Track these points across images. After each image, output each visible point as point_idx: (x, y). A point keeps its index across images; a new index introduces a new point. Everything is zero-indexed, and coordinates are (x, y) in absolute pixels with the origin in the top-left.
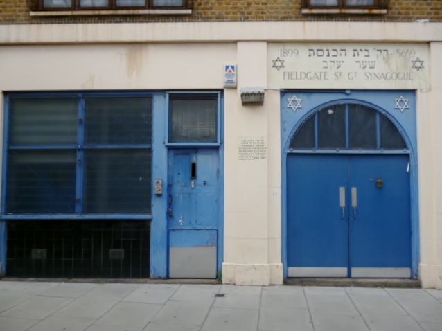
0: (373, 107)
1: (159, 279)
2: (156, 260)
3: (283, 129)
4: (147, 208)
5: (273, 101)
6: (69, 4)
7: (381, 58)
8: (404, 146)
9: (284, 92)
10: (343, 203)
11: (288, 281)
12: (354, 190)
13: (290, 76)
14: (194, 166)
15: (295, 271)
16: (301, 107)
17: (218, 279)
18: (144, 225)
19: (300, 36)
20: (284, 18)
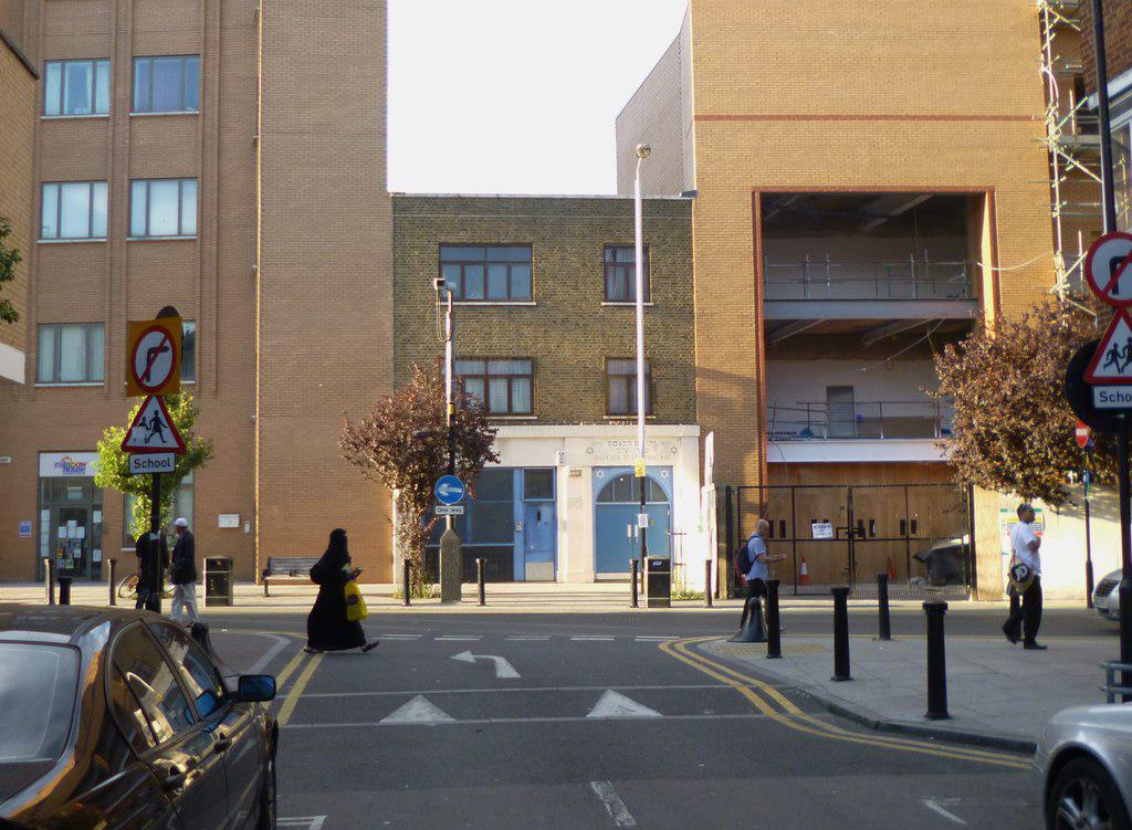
0: (759, 229)
1: (520, 581)
2: (517, 571)
3: (594, 490)
4: (511, 540)
5: (587, 473)
6: (51, 379)
7: (651, 448)
8: (666, 500)
9: (594, 468)
10: (629, 535)
11: (596, 581)
12: (629, 535)
13: (597, 458)
14: (539, 514)
15: (601, 576)
16: (604, 477)
17: (555, 580)
18: (510, 551)
19: (838, 306)
20: (884, 325)
